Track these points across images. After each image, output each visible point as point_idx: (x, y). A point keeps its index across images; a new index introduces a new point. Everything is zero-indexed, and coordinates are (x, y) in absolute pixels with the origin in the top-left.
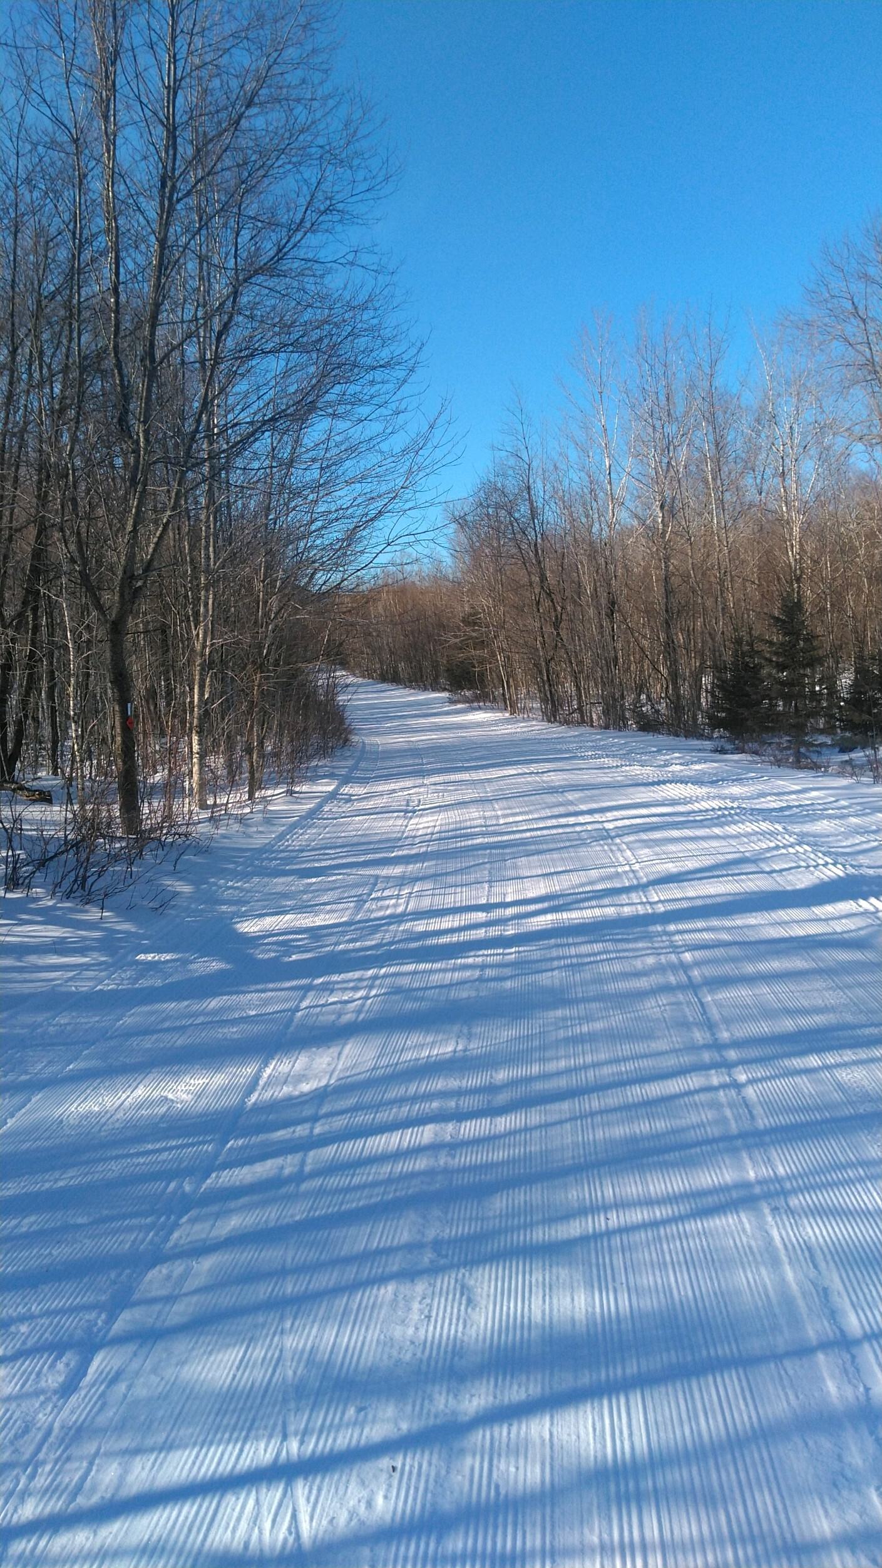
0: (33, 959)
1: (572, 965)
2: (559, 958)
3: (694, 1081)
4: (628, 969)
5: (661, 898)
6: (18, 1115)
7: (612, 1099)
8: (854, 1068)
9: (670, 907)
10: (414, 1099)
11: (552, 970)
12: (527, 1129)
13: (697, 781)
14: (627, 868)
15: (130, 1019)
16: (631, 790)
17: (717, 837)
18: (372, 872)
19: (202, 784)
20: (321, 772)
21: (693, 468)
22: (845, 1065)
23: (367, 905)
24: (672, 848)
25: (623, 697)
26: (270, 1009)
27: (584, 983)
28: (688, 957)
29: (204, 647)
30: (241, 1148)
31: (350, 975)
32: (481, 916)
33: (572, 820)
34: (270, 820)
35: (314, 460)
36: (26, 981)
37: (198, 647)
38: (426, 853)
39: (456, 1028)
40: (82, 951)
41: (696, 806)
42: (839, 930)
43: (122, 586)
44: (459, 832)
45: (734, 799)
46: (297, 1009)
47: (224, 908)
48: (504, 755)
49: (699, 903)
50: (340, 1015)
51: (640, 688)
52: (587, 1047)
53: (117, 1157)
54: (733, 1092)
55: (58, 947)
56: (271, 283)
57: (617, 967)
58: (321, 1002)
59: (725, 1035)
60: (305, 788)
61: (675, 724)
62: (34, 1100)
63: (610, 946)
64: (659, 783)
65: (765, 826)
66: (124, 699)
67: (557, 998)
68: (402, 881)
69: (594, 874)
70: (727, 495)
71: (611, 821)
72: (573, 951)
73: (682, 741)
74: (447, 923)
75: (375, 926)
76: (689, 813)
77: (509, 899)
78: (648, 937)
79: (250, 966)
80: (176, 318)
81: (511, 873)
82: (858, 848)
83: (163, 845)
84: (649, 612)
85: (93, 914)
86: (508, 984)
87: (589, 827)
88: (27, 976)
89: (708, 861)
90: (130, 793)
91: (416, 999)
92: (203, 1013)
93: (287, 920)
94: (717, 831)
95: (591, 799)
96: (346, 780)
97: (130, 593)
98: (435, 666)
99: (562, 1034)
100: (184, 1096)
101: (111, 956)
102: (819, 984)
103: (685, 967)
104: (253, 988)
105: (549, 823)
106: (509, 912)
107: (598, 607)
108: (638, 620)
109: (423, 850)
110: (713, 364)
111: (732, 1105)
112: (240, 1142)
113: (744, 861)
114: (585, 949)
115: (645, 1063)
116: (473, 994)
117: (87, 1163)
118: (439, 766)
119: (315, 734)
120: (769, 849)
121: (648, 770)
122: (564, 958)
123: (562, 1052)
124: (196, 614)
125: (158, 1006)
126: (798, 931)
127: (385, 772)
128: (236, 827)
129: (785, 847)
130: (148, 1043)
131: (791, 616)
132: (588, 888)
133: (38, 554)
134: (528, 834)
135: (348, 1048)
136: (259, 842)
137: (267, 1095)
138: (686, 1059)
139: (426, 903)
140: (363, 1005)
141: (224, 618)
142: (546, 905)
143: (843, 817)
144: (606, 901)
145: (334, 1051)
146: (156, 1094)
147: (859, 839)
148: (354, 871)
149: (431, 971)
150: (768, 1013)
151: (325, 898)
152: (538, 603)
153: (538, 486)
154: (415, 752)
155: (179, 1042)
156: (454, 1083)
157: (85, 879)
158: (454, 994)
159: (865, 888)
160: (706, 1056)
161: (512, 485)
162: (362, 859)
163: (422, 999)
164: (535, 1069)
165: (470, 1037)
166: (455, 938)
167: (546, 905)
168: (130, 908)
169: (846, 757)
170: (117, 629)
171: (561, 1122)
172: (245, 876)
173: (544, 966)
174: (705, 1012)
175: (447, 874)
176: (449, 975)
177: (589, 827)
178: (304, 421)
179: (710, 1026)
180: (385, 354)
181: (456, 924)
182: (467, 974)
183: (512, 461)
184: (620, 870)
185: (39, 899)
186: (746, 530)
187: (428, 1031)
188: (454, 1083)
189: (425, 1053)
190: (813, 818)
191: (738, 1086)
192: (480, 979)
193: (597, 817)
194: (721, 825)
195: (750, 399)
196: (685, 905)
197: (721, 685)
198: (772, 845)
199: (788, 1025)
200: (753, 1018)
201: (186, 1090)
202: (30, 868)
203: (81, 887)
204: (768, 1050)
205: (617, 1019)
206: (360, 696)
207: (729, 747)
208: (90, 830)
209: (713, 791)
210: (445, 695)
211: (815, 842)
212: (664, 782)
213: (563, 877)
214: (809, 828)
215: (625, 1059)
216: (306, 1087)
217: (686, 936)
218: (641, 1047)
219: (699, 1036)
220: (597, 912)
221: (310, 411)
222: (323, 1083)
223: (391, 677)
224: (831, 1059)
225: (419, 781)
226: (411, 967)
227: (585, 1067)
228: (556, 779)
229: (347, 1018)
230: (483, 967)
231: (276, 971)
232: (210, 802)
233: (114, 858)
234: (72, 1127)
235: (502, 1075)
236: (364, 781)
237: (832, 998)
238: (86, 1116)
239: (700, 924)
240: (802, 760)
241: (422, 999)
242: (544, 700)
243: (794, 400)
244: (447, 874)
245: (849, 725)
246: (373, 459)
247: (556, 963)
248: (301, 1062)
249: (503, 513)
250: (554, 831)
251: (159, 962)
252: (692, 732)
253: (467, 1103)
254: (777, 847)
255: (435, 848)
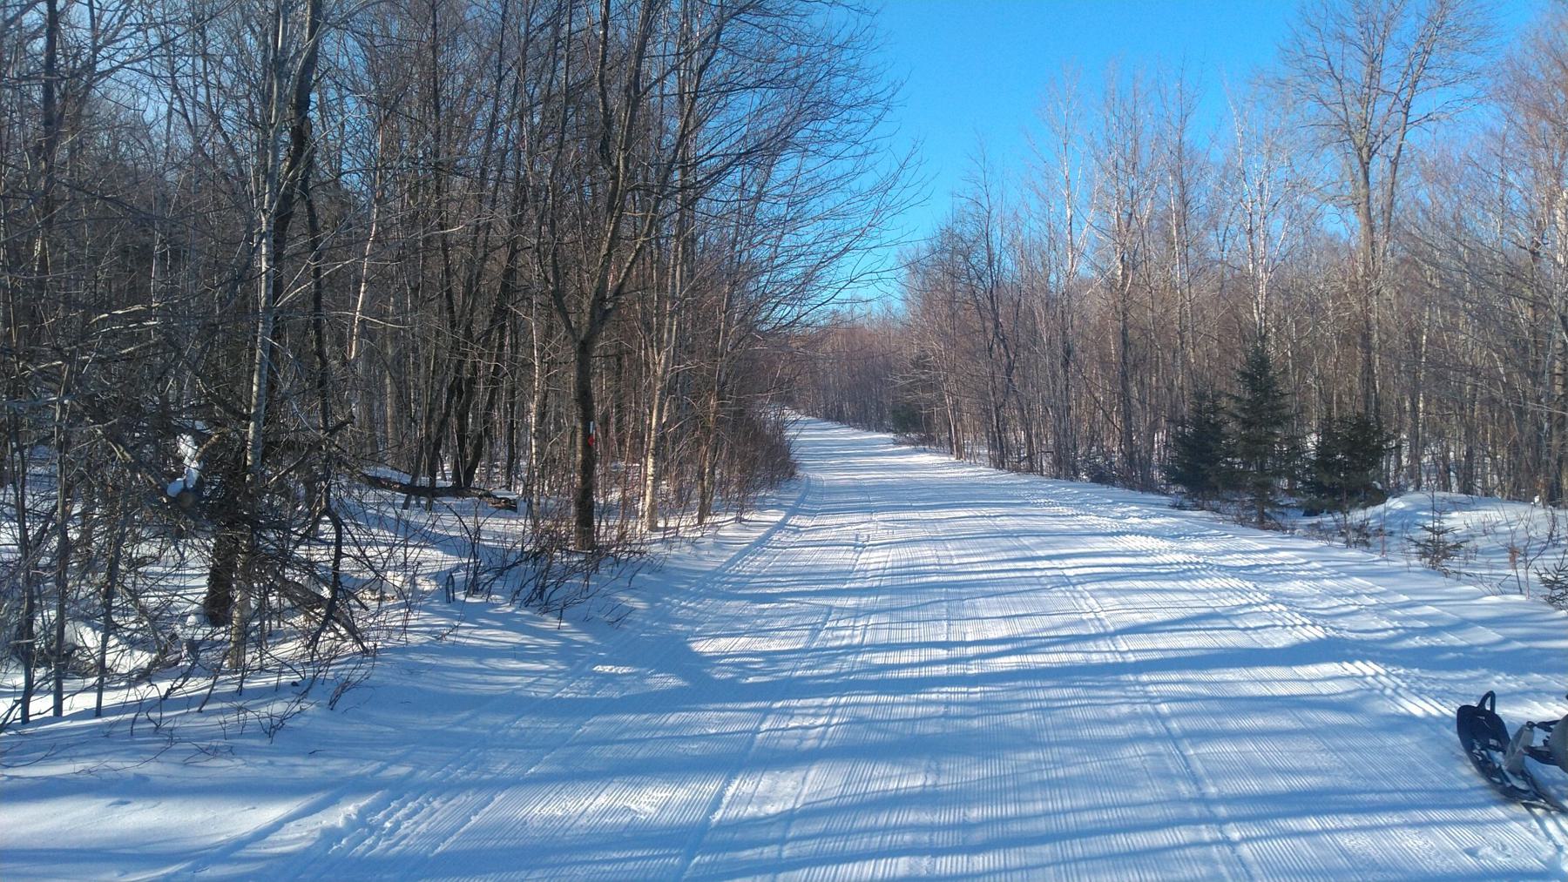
0: (493, 662)
1: (1041, 708)
2: (1028, 701)
3: (1183, 835)
4: (1102, 716)
5: (1131, 648)
6: (482, 813)
7: (1097, 845)
8: (1357, 834)
9: (1141, 657)
10: (885, 830)
11: (1022, 712)
12: (1006, 870)
13: (1157, 534)
14: (1092, 616)
15: (593, 726)
16: (1089, 539)
17: (1184, 591)
18: (825, 602)
19: (653, 507)
20: (768, 502)
21: (1155, 223)
22: (1347, 830)
23: (822, 634)
24: (1136, 598)
25: (1075, 447)
26: (729, 729)
27: (1056, 727)
28: (1164, 708)
29: (665, 372)
30: (707, 864)
31: (809, 702)
32: (942, 653)
33: (1030, 565)
34: (720, 545)
35: (783, 196)
36: (486, 683)
37: (660, 372)
38: (878, 588)
39: (924, 763)
40: (540, 658)
41: (1159, 559)
42: (1324, 692)
43: (593, 306)
44: (911, 570)
45: (1198, 554)
46: (757, 731)
47: (678, 627)
48: (950, 498)
49: (1172, 655)
50: (802, 739)
51: (1092, 440)
52: (1065, 791)
53: (582, 863)
54: (1227, 850)
55: (517, 652)
56: (755, 21)
57: (1090, 713)
58: (783, 726)
59: (1212, 790)
60: (754, 517)
61: (1128, 476)
62: (497, 799)
63: (1081, 692)
64: (1118, 534)
65: (1235, 583)
66: (587, 418)
67: (1027, 740)
68: (856, 613)
69: (1058, 619)
70: (1190, 250)
71: (1071, 568)
72: (1042, 694)
73: (1138, 495)
74: (906, 657)
75: (832, 655)
76: (1153, 565)
77: (969, 638)
78: (1120, 685)
79: (706, 685)
80: (663, 48)
81: (970, 613)
82: (1336, 611)
83: (618, 562)
84: (1104, 362)
85: (551, 623)
86: (975, 723)
87: (1049, 573)
88: (488, 678)
89: (1177, 614)
90: (586, 512)
91: (880, 731)
92: (662, 727)
93: (740, 644)
94: (1184, 584)
95: (1049, 545)
96: (793, 512)
97: (600, 315)
98: (880, 409)
99: (1036, 776)
100: (648, 809)
101: (570, 664)
102: (1310, 744)
103: (1160, 716)
104: (711, 706)
105: (997, 567)
106: (971, 651)
107: (1053, 355)
108: (1094, 370)
109: (876, 584)
110: (1184, 118)
111: (1227, 863)
112: (707, 858)
113: (1214, 616)
114: (1053, 693)
115: (1129, 812)
116: (939, 730)
117: (553, 866)
118: (886, 503)
119: (765, 466)
120: (1241, 606)
121: (1105, 521)
122: (1033, 700)
123: (1038, 795)
124: (660, 341)
125: (615, 717)
126: (1280, 690)
127: (833, 506)
128: (688, 549)
129: (1257, 604)
130: (609, 752)
131: (1258, 374)
132: (1052, 633)
133: (510, 273)
134: (985, 576)
135: (812, 773)
136: (710, 565)
137: (733, 813)
138: (1173, 812)
139: (882, 637)
140: (825, 733)
141: (685, 347)
142: (1009, 647)
143: (1316, 579)
144: (1073, 647)
145: (797, 775)
146: (618, 804)
147: (1335, 602)
148: (807, 599)
149: (893, 704)
150: (1258, 771)
151: (779, 624)
152: (991, 349)
153: (996, 234)
154: (859, 489)
155: (640, 754)
156: (925, 817)
157: (543, 588)
158: (919, 728)
159: (1349, 652)
160: (1194, 810)
161: (969, 231)
162: (814, 588)
163: (886, 731)
164: (1011, 810)
165: (939, 773)
166: (916, 673)
167: (1009, 647)
168: (587, 620)
169: (1315, 520)
170: (585, 349)
171: (1043, 866)
172: (698, 597)
173: (1011, 707)
174: (1188, 766)
175: (902, 609)
176: (912, 710)
177: (1049, 573)
178: (775, 155)
179: (1195, 779)
180: (864, 92)
181: (916, 660)
182: (932, 709)
183: (972, 209)
184: (1085, 617)
185: (498, 605)
186: (1207, 288)
187: (894, 764)
188: (925, 817)
189: (893, 785)
190: (1286, 579)
191: (1228, 842)
192: (946, 716)
193: (1056, 563)
194: (1188, 579)
195: (1218, 155)
196: (1157, 656)
197: (1181, 441)
198: (1244, 602)
199: (1280, 784)
200: (1240, 774)
201: (649, 802)
202: (491, 575)
203: (539, 598)
204: (1262, 809)
205: (1094, 765)
206: (808, 434)
207: (1188, 503)
208: (546, 545)
209: (1176, 545)
210: (890, 436)
211: (1290, 601)
212: (1124, 534)
213: (1025, 620)
214: (1280, 587)
215: (1106, 807)
216: (771, 809)
217: (1160, 687)
218: (1121, 796)
219: (1184, 789)
220: (1064, 657)
221: (783, 148)
222: (789, 806)
223: (836, 416)
224: (1330, 822)
225: (867, 517)
226: (872, 699)
227: (1065, 812)
228: (1010, 523)
229: (810, 743)
230: (948, 704)
231: (733, 692)
232: (661, 524)
233: (571, 570)
234: (537, 830)
235: (975, 814)
236: (811, 514)
237: (1323, 760)
238: (551, 819)
239: (1174, 676)
240: (1264, 518)
241: (886, 731)
242: (992, 447)
243: (1266, 158)
244: (902, 609)
245: (1318, 488)
246: (840, 197)
247: (1024, 706)
248: (765, 782)
249: (960, 258)
250: (1012, 575)
251: (616, 675)
252: (1148, 486)
253: (940, 838)
254: (1249, 605)
255: (889, 583)
